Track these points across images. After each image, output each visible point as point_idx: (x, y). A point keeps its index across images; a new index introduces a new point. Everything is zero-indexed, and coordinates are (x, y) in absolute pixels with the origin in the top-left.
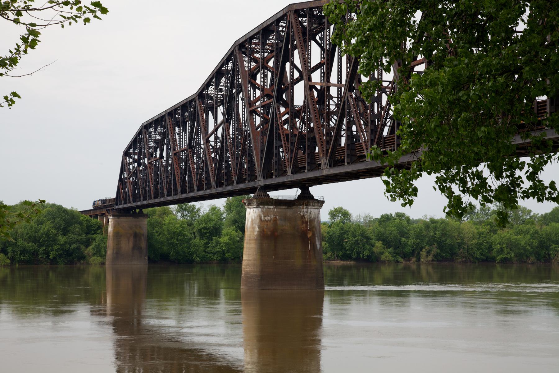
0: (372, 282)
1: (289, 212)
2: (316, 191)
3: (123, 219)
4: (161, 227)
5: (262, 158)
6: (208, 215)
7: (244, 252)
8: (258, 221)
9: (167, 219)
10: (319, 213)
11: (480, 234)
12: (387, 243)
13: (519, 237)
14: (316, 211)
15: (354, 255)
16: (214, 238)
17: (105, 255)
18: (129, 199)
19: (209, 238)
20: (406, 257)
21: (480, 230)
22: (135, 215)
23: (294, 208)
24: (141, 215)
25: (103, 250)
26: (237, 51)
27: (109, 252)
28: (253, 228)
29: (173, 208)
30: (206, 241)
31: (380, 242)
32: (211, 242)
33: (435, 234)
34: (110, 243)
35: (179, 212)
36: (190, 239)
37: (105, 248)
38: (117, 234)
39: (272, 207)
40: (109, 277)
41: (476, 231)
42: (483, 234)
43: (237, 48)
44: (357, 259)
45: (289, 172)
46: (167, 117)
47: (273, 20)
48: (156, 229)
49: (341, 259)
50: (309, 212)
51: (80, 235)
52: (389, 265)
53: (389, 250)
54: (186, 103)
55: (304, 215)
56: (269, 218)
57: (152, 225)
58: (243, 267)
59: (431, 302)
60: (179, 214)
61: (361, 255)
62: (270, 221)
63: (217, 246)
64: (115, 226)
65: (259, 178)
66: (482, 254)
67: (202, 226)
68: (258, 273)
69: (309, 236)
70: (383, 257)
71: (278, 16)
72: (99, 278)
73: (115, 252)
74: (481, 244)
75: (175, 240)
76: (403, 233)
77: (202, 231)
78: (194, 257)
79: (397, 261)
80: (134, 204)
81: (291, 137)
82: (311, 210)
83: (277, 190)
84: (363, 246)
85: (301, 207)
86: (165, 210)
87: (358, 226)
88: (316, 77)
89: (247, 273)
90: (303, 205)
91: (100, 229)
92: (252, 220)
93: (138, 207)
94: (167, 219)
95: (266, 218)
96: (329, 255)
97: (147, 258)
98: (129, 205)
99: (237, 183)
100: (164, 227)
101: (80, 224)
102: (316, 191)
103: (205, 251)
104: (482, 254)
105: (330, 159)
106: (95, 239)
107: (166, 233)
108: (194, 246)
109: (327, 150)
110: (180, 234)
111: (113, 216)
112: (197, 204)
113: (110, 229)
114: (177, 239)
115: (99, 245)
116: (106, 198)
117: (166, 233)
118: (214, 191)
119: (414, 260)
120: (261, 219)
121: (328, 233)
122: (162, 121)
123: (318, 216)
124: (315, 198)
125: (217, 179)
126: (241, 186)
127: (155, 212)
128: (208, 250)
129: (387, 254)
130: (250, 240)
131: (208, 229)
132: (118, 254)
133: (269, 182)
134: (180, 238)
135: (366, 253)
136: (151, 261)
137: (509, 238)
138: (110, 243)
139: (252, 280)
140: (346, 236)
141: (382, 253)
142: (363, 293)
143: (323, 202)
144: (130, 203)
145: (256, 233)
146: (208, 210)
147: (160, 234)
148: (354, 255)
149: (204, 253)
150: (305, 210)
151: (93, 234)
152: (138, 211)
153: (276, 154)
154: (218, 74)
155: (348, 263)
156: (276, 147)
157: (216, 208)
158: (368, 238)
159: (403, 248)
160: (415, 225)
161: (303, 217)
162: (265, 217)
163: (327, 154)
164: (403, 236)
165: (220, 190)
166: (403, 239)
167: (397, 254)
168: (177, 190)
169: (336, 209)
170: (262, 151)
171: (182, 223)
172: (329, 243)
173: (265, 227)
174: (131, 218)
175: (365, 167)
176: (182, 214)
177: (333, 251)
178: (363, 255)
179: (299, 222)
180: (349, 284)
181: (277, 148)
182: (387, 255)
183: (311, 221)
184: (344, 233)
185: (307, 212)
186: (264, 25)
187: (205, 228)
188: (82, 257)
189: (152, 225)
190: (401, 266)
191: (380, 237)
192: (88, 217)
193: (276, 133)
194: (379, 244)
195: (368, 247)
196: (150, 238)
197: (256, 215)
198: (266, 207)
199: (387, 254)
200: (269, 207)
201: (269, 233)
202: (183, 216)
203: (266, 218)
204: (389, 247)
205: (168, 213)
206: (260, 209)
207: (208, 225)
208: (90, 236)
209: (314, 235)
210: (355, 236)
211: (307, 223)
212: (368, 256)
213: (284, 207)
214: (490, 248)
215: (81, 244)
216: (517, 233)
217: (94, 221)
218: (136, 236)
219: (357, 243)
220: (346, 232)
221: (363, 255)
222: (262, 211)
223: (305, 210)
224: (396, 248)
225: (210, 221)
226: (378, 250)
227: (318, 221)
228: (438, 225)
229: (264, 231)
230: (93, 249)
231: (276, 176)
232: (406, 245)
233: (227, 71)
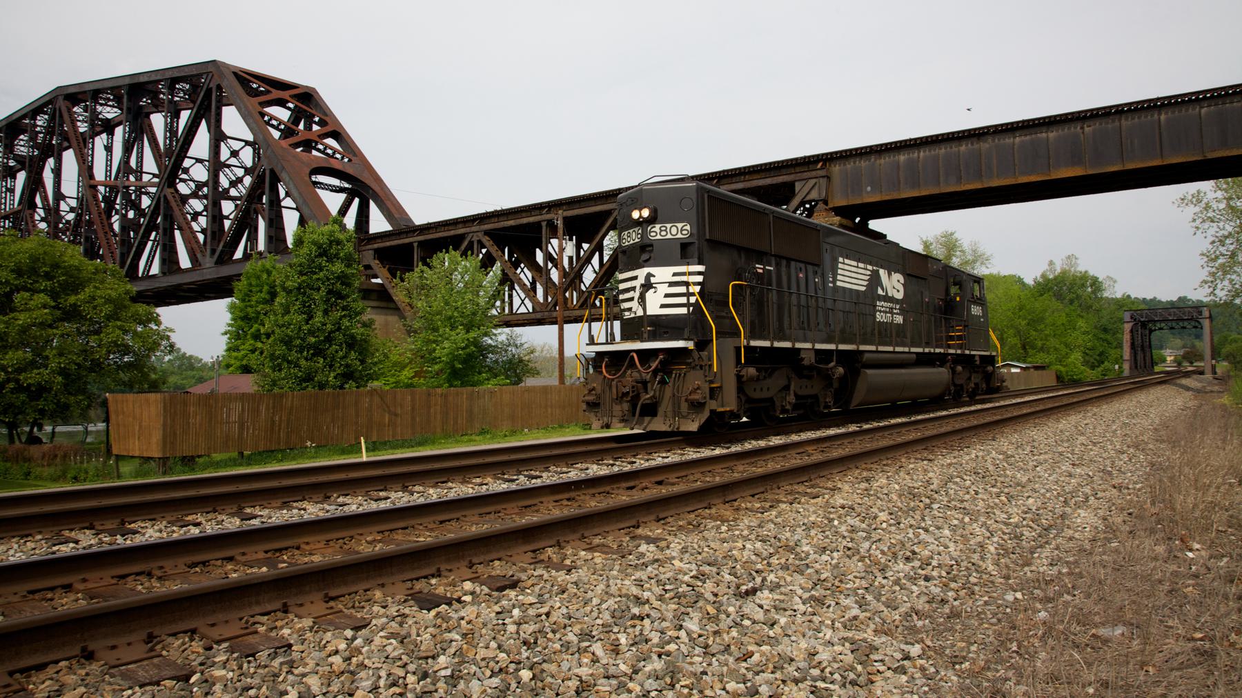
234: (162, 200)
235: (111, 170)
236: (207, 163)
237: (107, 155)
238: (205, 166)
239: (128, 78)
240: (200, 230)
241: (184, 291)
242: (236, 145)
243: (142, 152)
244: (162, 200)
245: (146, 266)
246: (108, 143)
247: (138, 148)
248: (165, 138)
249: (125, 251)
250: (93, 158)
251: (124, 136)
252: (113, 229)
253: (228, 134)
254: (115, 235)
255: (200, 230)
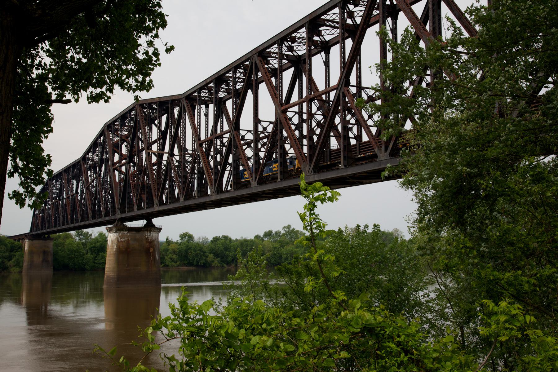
0: (206, 280)
1: (138, 236)
2: (156, 221)
3: (36, 242)
4: (64, 247)
5: (119, 200)
6: (96, 238)
7: (106, 263)
8: (116, 241)
9: (68, 241)
10: (158, 236)
11: (275, 248)
12: (216, 255)
13: (297, 249)
14: (156, 234)
15: (195, 263)
16: (100, 253)
17: (22, 266)
18: (39, 228)
19: (98, 253)
20: (228, 263)
21: (275, 246)
22: (45, 239)
23: (141, 233)
24: (49, 238)
25: (21, 263)
26: (106, 130)
27: (25, 264)
28: (113, 246)
29: (73, 233)
30: (95, 255)
31: (212, 254)
32: (98, 256)
33: (247, 249)
34: (26, 258)
35: (78, 236)
36: (84, 255)
37: (23, 261)
38: (31, 252)
39: (126, 232)
40: (25, 281)
41: (272, 246)
42: (276, 248)
43: (106, 128)
44: (197, 266)
45: (135, 209)
46: (63, 173)
47: (127, 110)
48: (60, 248)
49: (187, 266)
50: (151, 235)
51: (4, 252)
52: (217, 269)
53: (217, 259)
54: (75, 164)
55: (148, 238)
56: (124, 240)
57: (57, 246)
58: (106, 272)
59: (86, 315)
60: (77, 238)
61: (199, 263)
62: (124, 241)
63: (102, 258)
64: (30, 246)
65: (118, 213)
66: (275, 261)
67: (92, 246)
68: (116, 276)
69: (151, 251)
70: (213, 264)
71: (130, 108)
72: (18, 282)
73: (29, 264)
74: (275, 255)
75: (73, 256)
76: (227, 248)
77: (93, 249)
78: (87, 267)
79: (223, 266)
80: (42, 231)
81: (137, 186)
82: (153, 234)
83: (132, 221)
84: (201, 257)
85: (146, 232)
86: (67, 235)
87: (197, 244)
88: (155, 147)
89: (108, 276)
90: (147, 231)
91: (21, 248)
92: (112, 241)
93: (45, 233)
94: (68, 241)
95: (122, 240)
96: (178, 263)
97: (52, 267)
98: (39, 232)
99: (105, 216)
100: (66, 247)
101: (6, 245)
102: (156, 221)
103: (94, 262)
104: (275, 261)
105: (159, 200)
106: (16, 256)
107: (66, 250)
108: (86, 259)
109: (158, 195)
110: (77, 251)
111: (29, 239)
112: (89, 230)
113: (26, 248)
114: (75, 255)
115: (18, 259)
116: (242, 237)
117: (66, 250)
118: (91, 222)
119: (233, 265)
120: (118, 240)
121: (178, 249)
122: (60, 176)
123: (157, 238)
124: (156, 226)
125: (93, 214)
126: (107, 218)
127: (60, 236)
128: (97, 261)
129: (216, 262)
130: (110, 254)
131: (97, 247)
132: (31, 265)
133: (124, 215)
134: (76, 254)
135: (203, 261)
136: (55, 269)
137: (292, 250)
138: (26, 258)
139: (112, 281)
140: (189, 251)
141: (213, 261)
142: (200, 287)
143: (161, 229)
144: (39, 230)
145: (114, 250)
146: (97, 235)
147: (62, 251)
148: (195, 263)
149: (93, 264)
150: (149, 234)
151: (15, 252)
152: (46, 236)
153: (128, 197)
154: (94, 145)
155: (191, 268)
156: (128, 192)
157: (102, 233)
158: (204, 252)
159: (227, 258)
160: (234, 243)
161: (147, 239)
162: (121, 239)
163: (158, 197)
164: (227, 250)
165: (94, 221)
166: (227, 252)
167: (223, 262)
168: (68, 222)
169: (184, 234)
170: (120, 195)
171: (78, 244)
172: (179, 255)
173: (121, 245)
174: (41, 241)
175: (179, 206)
176: (79, 237)
177: (181, 261)
178: (201, 263)
179: (145, 242)
180: (191, 282)
181: (129, 193)
182: (216, 262)
183: (153, 241)
184: (189, 249)
185: (150, 235)
186: (122, 114)
187: (94, 247)
188: (6, 268)
189: (57, 246)
190: (225, 269)
191: (212, 251)
192: (12, 240)
193: (128, 183)
194: (211, 256)
195: (204, 258)
196: (55, 254)
197: (115, 238)
198: (122, 232)
199: (216, 262)
200: (124, 232)
201: (124, 250)
202: (80, 239)
203: (122, 240)
204: (217, 258)
205: (70, 236)
206: (118, 234)
207: (97, 245)
208: (13, 253)
209: (154, 250)
210: (195, 251)
211: (150, 242)
212: (204, 264)
213: (134, 232)
214: (281, 257)
215: (5, 259)
216: (296, 247)
217: (17, 243)
218: (45, 253)
219: (197, 255)
220: (190, 248)
221: (201, 263)
222: (119, 235)
223: (149, 234)
224: (222, 258)
225: (98, 242)
226: (211, 260)
227: (157, 241)
228: (249, 243)
229: (120, 248)
230: (14, 262)
231: (128, 212)
232: (228, 256)
233: (100, 143)
234: (254, 64)
235: (208, 130)
236: (253, 132)
237: (206, 119)
238: (252, 134)
239: (213, 76)
240: (353, 137)
241: (244, 198)
242: (265, 124)
243: (223, 122)
244: (254, 64)
245: (227, 182)
246: (206, 112)
247: (221, 121)
248: (233, 113)
249: (257, 167)
250: (200, 130)
251: (214, 112)
252: (210, 165)
253: (261, 120)
254: (212, 169)
255: (353, 137)
